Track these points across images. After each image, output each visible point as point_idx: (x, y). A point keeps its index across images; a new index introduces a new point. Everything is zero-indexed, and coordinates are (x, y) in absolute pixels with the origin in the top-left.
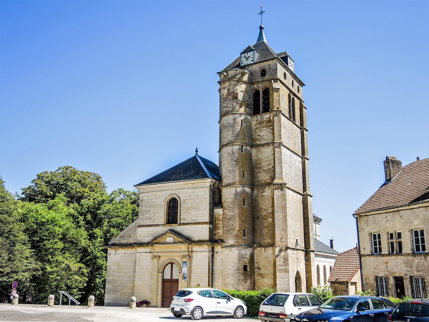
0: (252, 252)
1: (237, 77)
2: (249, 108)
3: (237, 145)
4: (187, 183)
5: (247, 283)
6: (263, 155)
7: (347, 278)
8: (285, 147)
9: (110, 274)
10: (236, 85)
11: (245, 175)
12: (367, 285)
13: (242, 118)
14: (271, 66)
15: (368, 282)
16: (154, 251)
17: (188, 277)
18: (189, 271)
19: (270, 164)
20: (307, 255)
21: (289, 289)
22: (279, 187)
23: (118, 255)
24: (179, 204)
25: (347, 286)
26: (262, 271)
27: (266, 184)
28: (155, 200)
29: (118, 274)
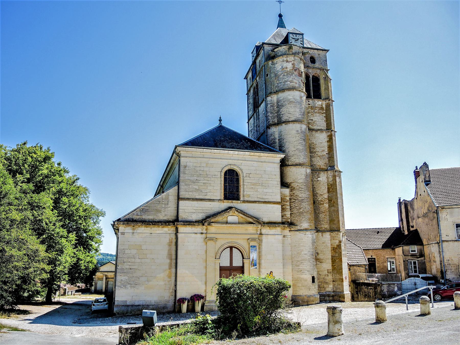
23: (138, 235)
27: (320, 170)
28: (206, 169)
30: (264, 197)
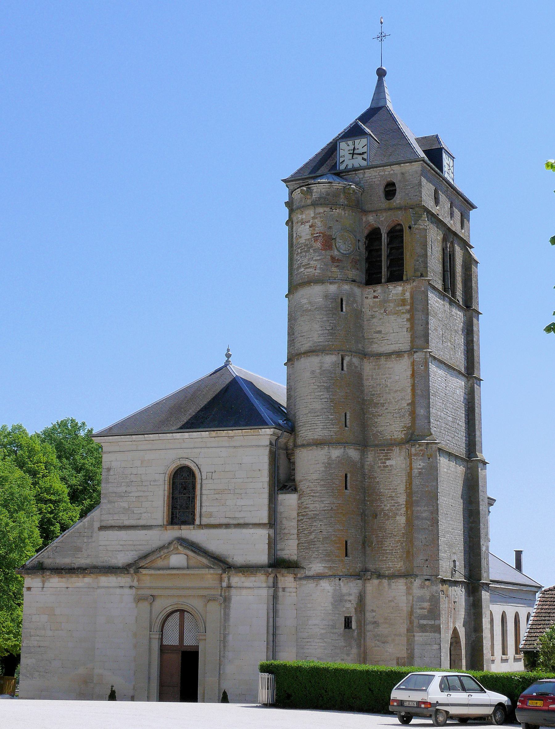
0: (361, 588)
4: (217, 435)
5: (351, 656)
9: (32, 634)
24: (198, 481)
29: (50, 633)
30: (237, 515)
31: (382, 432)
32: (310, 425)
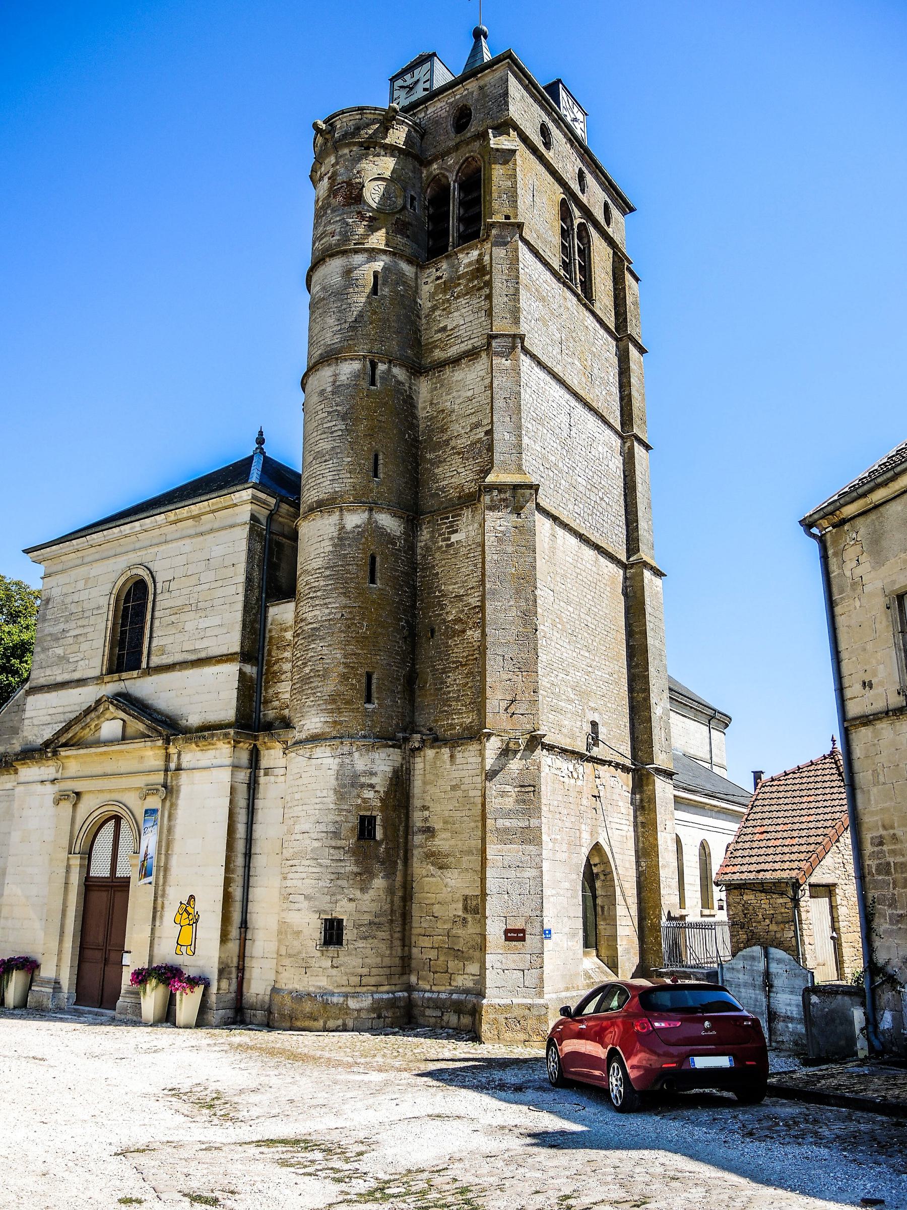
1: (362, 132)
2: (408, 237)
3: (351, 359)
5: (371, 892)
6: (455, 394)
7: (795, 865)
8: (533, 357)
10: (359, 159)
11: (380, 467)
12: (888, 873)
13: (378, 265)
14: (488, 89)
15: (891, 860)
16: (66, 776)
17: (158, 867)
18: (164, 844)
19: (477, 425)
20: (642, 786)
21: (538, 913)
22: (504, 500)
25: (796, 901)
26: (442, 842)
27: (462, 500)
28: (84, 596)
31: (445, 488)
32: (314, 479)
